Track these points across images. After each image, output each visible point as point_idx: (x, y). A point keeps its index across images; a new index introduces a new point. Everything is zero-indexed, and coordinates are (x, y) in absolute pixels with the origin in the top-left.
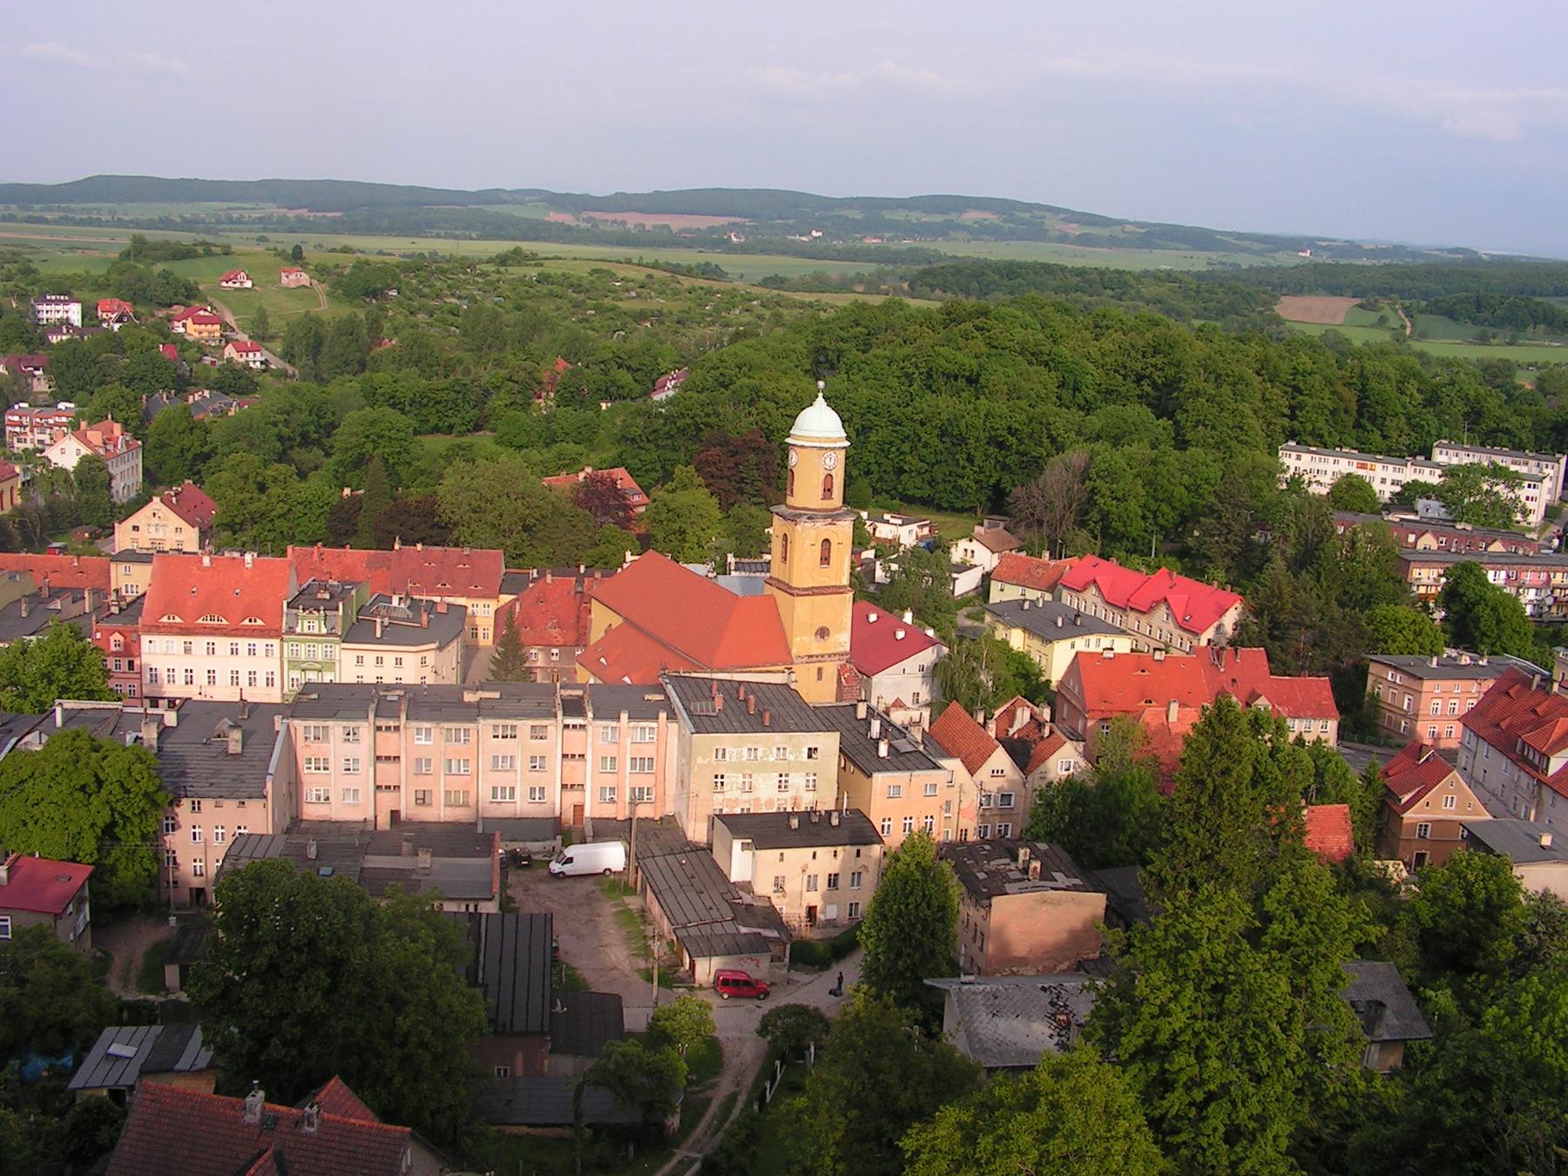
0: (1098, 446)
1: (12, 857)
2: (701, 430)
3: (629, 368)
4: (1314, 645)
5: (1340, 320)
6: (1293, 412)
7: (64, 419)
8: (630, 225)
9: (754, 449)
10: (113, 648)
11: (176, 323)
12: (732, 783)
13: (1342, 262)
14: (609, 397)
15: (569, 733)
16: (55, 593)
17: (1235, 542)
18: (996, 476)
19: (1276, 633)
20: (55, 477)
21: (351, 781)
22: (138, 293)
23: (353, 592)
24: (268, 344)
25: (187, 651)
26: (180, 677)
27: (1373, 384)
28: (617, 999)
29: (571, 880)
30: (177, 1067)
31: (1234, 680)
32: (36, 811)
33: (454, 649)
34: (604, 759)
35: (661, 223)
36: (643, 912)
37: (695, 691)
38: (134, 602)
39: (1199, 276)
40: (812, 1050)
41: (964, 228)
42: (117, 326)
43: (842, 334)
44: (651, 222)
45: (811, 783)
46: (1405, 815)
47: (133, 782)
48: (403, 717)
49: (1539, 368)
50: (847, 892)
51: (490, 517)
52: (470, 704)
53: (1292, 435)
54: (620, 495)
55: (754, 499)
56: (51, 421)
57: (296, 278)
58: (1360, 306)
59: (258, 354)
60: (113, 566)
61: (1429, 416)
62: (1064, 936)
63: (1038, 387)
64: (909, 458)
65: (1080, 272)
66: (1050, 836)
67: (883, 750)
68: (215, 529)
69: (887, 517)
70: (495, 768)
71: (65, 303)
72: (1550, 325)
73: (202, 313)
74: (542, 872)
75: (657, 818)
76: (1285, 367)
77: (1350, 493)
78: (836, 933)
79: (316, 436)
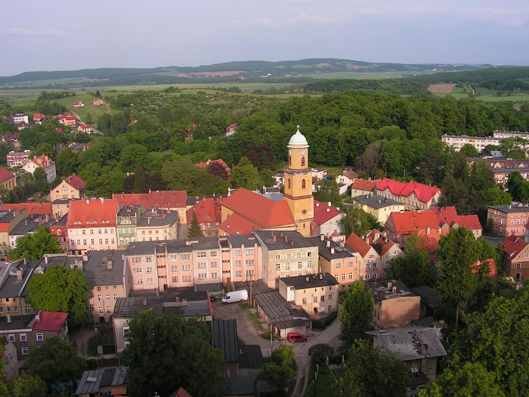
0: (383, 140)
1: (40, 311)
2: (246, 144)
3: (216, 125)
4: (467, 204)
5: (450, 91)
6: (445, 124)
7: (27, 156)
8: (206, 76)
9: (265, 150)
10: (58, 234)
11: (60, 120)
12: (283, 267)
13: (448, 71)
14: (211, 135)
15: (224, 253)
16: (36, 216)
17: (433, 170)
18: (348, 153)
19: (454, 200)
20: (27, 176)
21: (150, 276)
22: (46, 111)
23: (139, 209)
24: (92, 125)
25: (84, 233)
26: (82, 242)
27: (471, 113)
28: (258, 346)
29: (230, 304)
30: (113, 384)
31: (445, 218)
32: (46, 295)
33: (175, 225)
34: (237, 261)
35: (217, 75)
36: (257, 313)
37: (266, 236)
38: (63, 217)
39: (400, 79)
40: (328, 359)
41: (319, 69)
42: (40, 123)
43: (290, 108)
44: (213, 74)
45: (309, 265)
46: (512, 261)
47: (78, 282)
48: (166, 252)
49: (519, 103)
50: (328, 302)
51: (180, 180)
52: (188, 246)
53: (445, 132)
54: (223, 169)
55: (266, 167)
56: (22, 157)
57: (98, 102)
58: (457, 86)
59: (89, 129)
60: (53, 205)
61: (491, 122)
62: (407, 312)
63: (359, 122)
64: (317, 149)
65: (361, 81)
66: (395, 278)
67: (333, 251)
68: (85, 190)
69: (312, 169)
70: (199, 267)
71: (22, 116)
72: (521, 88)
73: (69, 116)
74: (219, 302)
75: (256, 280)
76: (441, 109)
77: (468, 150)
78: (326, 316)
79: (113, 155)
